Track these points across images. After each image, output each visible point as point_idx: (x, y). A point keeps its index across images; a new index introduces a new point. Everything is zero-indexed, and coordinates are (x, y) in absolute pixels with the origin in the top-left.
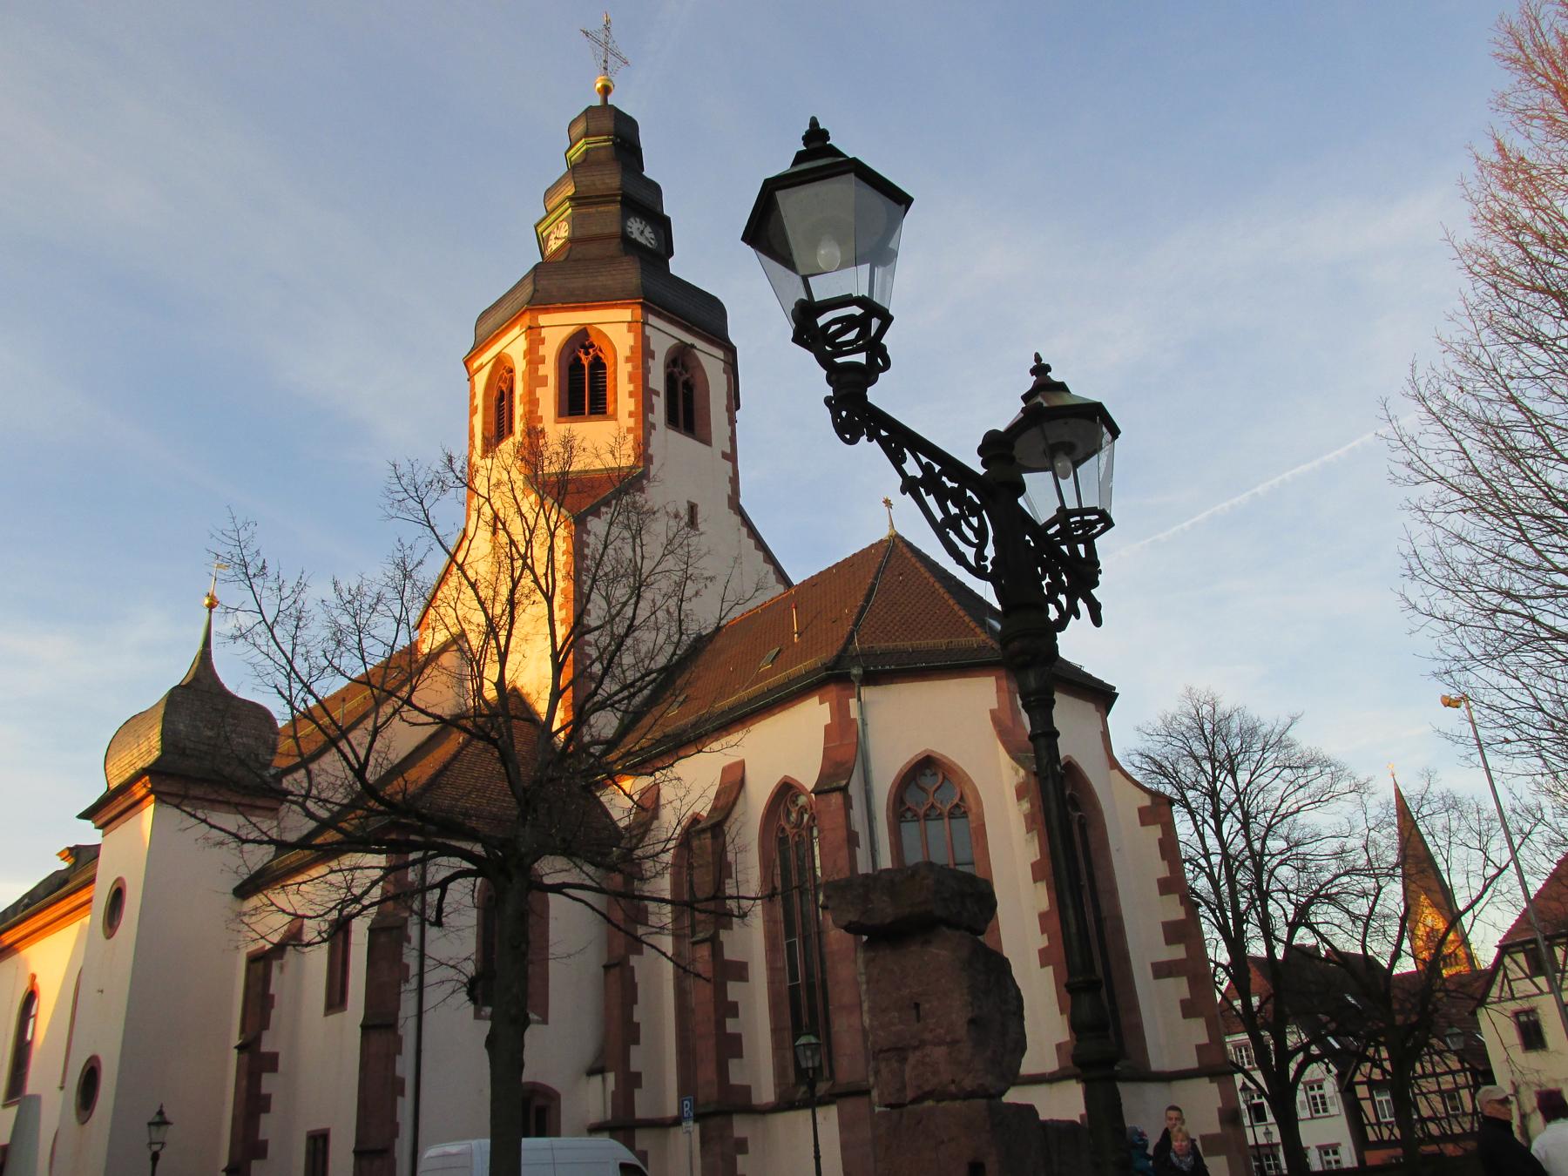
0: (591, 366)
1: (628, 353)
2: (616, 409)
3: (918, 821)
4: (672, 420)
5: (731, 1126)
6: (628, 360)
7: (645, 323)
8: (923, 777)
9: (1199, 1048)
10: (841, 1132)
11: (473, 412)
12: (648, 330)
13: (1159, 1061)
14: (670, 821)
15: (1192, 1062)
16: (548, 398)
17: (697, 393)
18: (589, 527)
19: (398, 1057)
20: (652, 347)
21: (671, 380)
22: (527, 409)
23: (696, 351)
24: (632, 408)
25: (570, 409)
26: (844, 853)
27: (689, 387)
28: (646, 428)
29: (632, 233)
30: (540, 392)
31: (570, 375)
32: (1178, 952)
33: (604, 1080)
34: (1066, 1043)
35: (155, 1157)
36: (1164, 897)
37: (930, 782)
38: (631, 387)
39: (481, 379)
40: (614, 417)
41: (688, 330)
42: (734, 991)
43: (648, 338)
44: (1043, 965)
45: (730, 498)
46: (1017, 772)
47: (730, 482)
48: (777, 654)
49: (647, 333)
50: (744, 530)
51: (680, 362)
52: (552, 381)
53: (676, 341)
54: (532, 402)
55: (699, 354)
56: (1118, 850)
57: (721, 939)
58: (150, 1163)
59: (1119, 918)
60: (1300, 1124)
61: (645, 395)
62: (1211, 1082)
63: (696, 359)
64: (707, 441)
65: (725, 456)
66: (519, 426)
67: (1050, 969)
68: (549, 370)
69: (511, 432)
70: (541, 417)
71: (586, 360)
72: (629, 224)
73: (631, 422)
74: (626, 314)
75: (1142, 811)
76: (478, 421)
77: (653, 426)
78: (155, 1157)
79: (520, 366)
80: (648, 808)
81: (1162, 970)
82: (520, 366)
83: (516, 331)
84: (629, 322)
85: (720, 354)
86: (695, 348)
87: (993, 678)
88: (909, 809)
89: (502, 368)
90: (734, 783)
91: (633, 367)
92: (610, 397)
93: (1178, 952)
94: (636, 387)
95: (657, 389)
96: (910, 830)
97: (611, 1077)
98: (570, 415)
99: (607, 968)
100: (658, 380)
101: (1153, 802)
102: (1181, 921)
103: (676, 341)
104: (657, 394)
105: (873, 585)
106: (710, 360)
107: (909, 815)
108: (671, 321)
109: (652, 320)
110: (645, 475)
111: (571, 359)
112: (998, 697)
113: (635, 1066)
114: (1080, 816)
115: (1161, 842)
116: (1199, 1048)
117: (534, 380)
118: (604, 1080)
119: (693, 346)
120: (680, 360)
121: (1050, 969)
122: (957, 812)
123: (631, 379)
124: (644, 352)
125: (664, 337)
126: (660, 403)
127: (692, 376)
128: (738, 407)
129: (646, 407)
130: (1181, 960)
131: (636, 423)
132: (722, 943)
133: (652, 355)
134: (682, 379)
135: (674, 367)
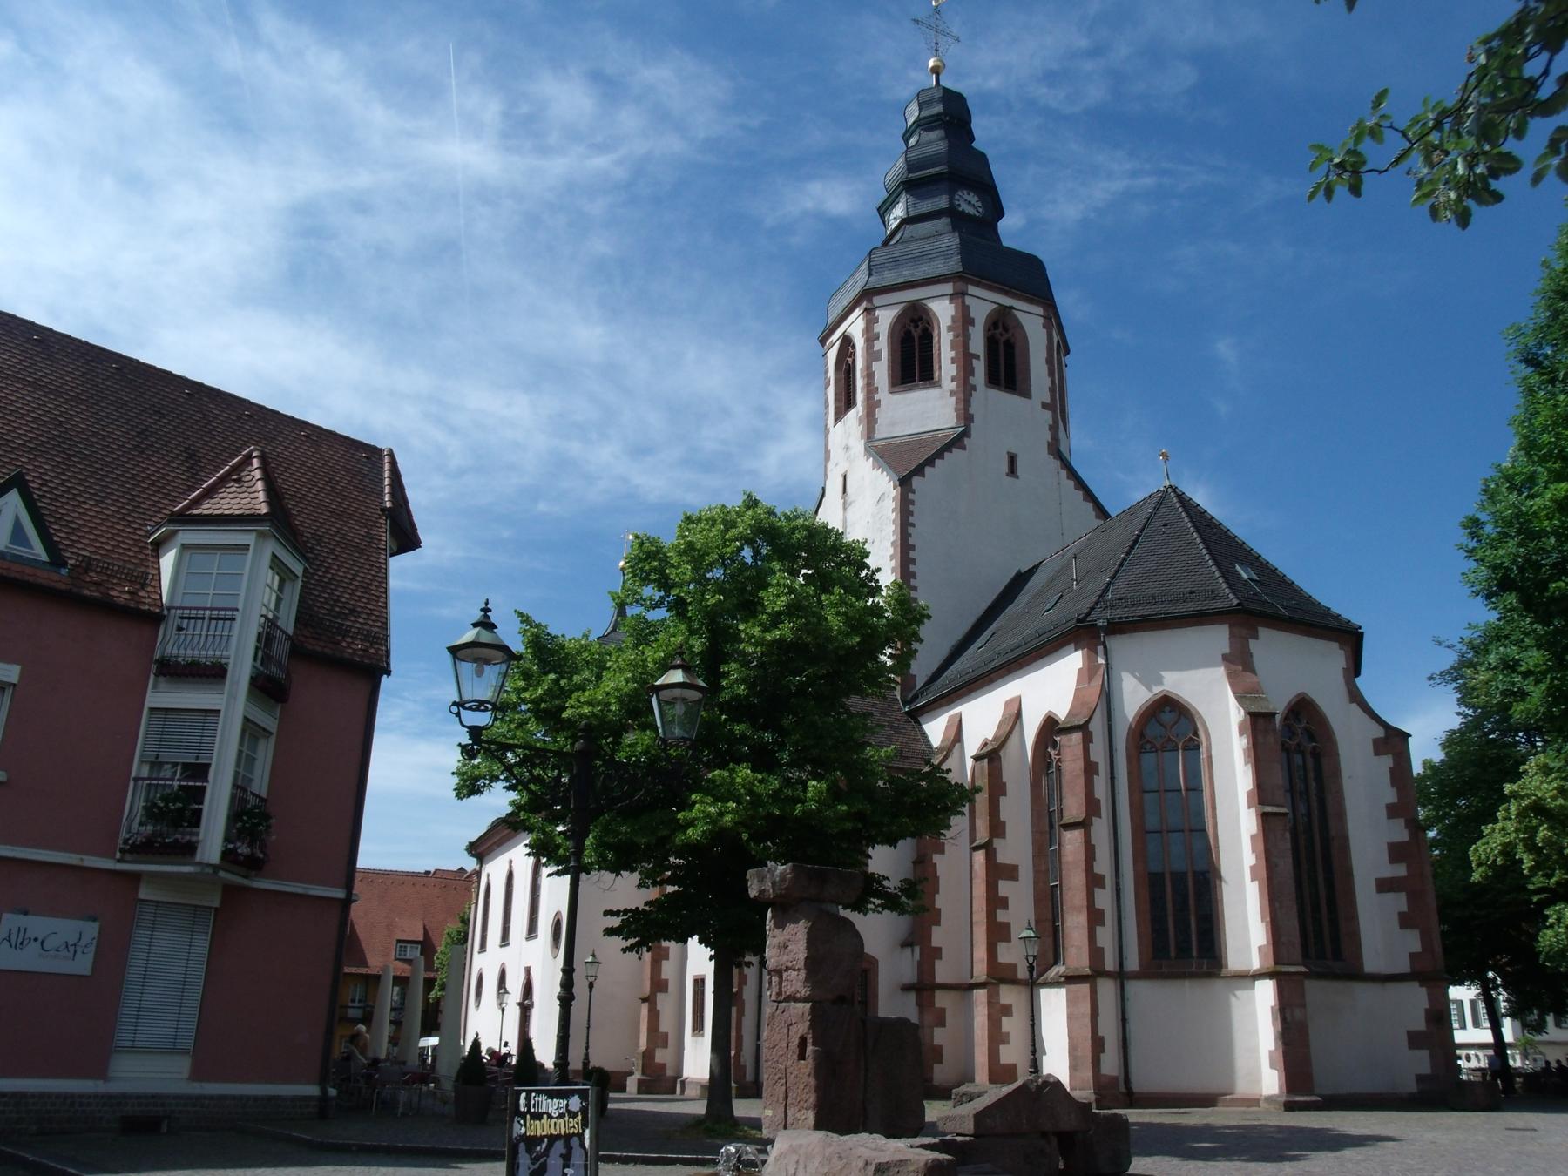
0: (920, 338)
1: (949, 323)
2: (940, 375)
3: (1156, 751)
4: (993, 380)
5: (998, 994)
6: (950, 329)
7: (964, 294)
8: (1163, 714)
9: (1413, 956)
10: (1068, 1007)
11: (828, 385)
12: (968, 300)
13: (1371, 964)
14: (972, 746)
15: (1404, 967)
16: (882, 369)
17: (1017, 351)
18: (914, 487)
19: (937, 896)
20: (972, 315)
21: (991, 343)
22: (866, 382)
23: (1014, 311)
24: (954, 373)
25: (902, 379)
26: (1081, 781)
27: (1010, 346)
28: (966, 392)
29: (959, 205)
30: (876, 366)
31: (902, 347)
32: (1401, 870)
33: (913, 951)
34: (1264, 946)
35: (591, 986)
36: (1391, 820)
37: (1167, 717)
38: (953, 354)
39: (832, 355)
40: (938, 385)
41: (1006, 293)
42: (1005, 888)
43: (968, 307)
44: (1252, 881)
45: (1049, 445)
46: (1239, 713)
47: (1050, 430)
48: (1059, 599)
49: (967, 303)
50: (1064, 473)
51: (1000, 325)
52: (885, 355)
53: (995, 306)
54: (870, 376)
55: (1019, 315)
56: (1350, 777)
57: (994, 846)
58: (588, 989)
59: (1345, 839)
60: (1455, 1031)
61: (965, 361)
62: (1421, 986)
63: (1017, 320)
64: (1026, 394)
65: (1044, 406)
66: (860, 396)
67: (1256, 883)
68: (883, 345)
69: (855, 404)
70: (953, 363)
71: (916, 334)
72: (957, 197)
73: (953, 386)
74: (948, 288)
75: (1376, 742)
76: (831, 391)
77: (974, 388)
78: (591, 986)
79: (860, 343)
80: (956, 736)
81: (1384, 886)
82: (860, 343)
83: (857, 312)
84: (950, 295)
85: (1040, 310)
86: (1014, 308)
87: (1227, 626)
88: (1148, 742)
89: (847, 341)
90: (1014, 716)
91: (954, 336)
92: (936, 366)
93: (1401, 870)
94: (957, 354)
95: (978, 353)
96: (1149, 759)
97: (917, 949)
98: (903, 383)
99: (914, 863)
100: (978, 345)
101: (1386, 733)
102: (1407, 842)
103: (995, 306)
104: (977, 357)
105: (1139, 536)
106: (1030, 320)
107: (1148, 746)
108: (990, 288)
109: (972, 289)
110: (965, 433)
111: (902, 333)
112: (1231, 643)
113: (935, 943)
114: (1314, 748)
115: (1392, 771)
116: (1413, 956)
117: (872, 356)
118: (913, 951)
119: (1012, 308)
120: (1001, 324)
121: (1256, 883)
122: (1191, 745)
123: (952, 348)
124: (964, 321)
125: (983, 303)
126: (980, 367)
127: (1013, 335)
128: (1067, 352)
129: (966, 369)
130: (1402, 877)
131: (958, 386)
132: (995, 849)
133: (971, 322)
134: (1002, 339)
135: (995, 329)
